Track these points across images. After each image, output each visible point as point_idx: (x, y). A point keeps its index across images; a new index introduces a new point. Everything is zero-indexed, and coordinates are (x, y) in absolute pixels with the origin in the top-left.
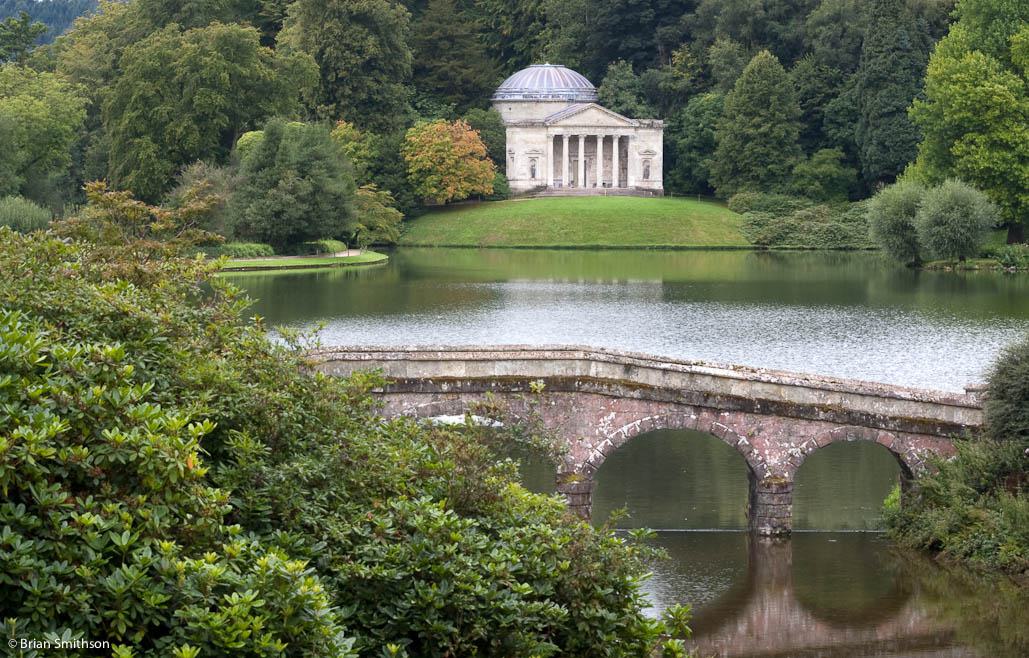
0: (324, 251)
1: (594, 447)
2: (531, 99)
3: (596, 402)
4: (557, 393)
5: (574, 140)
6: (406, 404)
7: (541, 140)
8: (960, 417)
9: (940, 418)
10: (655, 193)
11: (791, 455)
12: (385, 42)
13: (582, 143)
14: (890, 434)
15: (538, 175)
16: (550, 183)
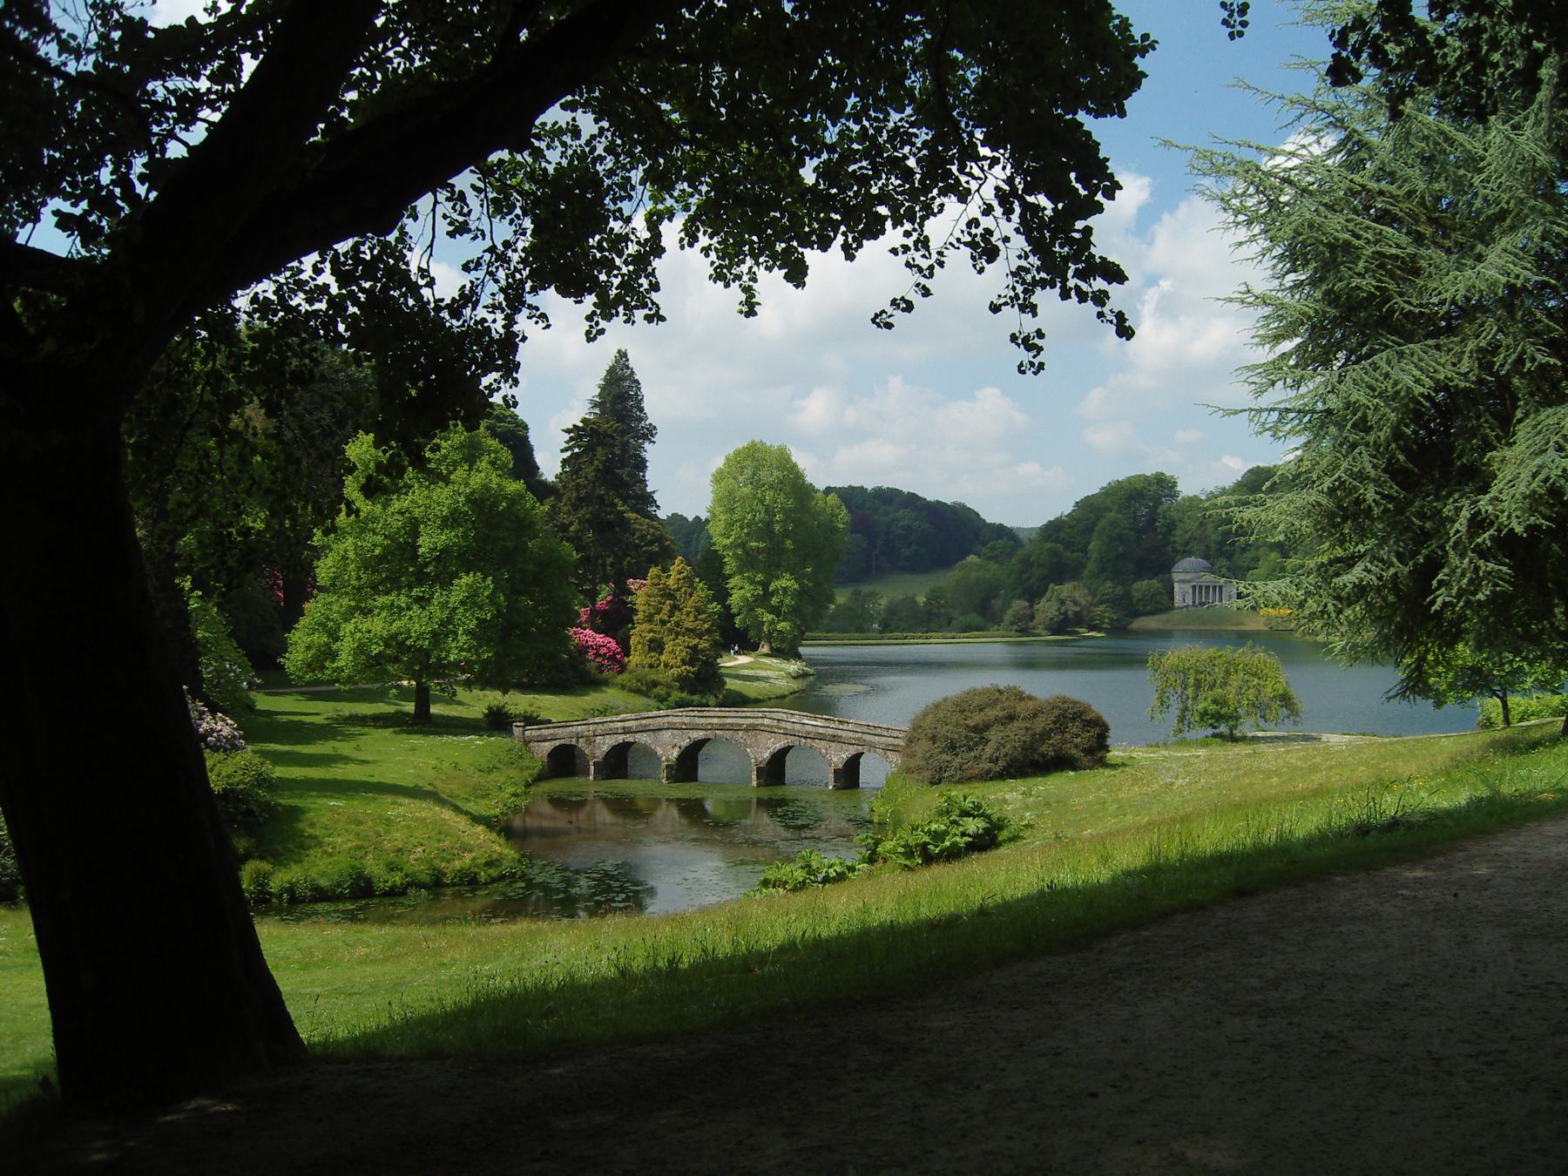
7: (1188, 588)
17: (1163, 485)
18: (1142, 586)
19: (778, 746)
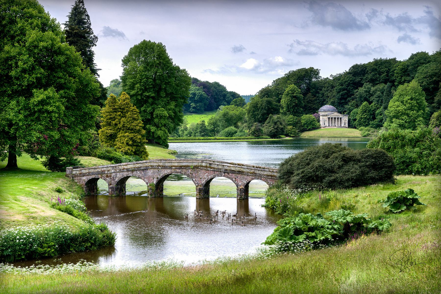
0: (280, 137)
2: (325, 111)
3: (203, 171)
5: (332, 118)
7: (326, 118)
8: (275, 174)
12: (299, 101)
17: (313, 68)
18: (305, 117)
19: (245, 182)
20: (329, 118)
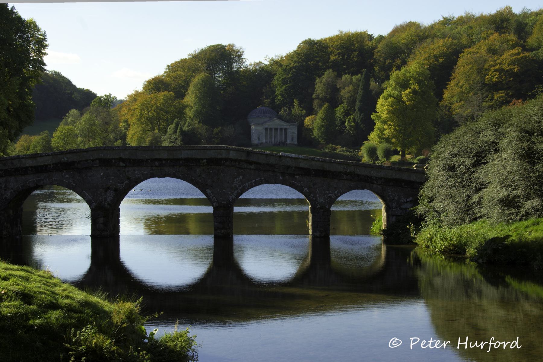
1: (232, 193)
4: (213, 167)
5: (271, 129)
6: (137, 172)
9: (404, 178)
10: (295, 145)
11: (330, 197)
13: (269, 130)
14: (379, 186)
15: (261, 139)
16: (264, 142)
20: (266, 129)
